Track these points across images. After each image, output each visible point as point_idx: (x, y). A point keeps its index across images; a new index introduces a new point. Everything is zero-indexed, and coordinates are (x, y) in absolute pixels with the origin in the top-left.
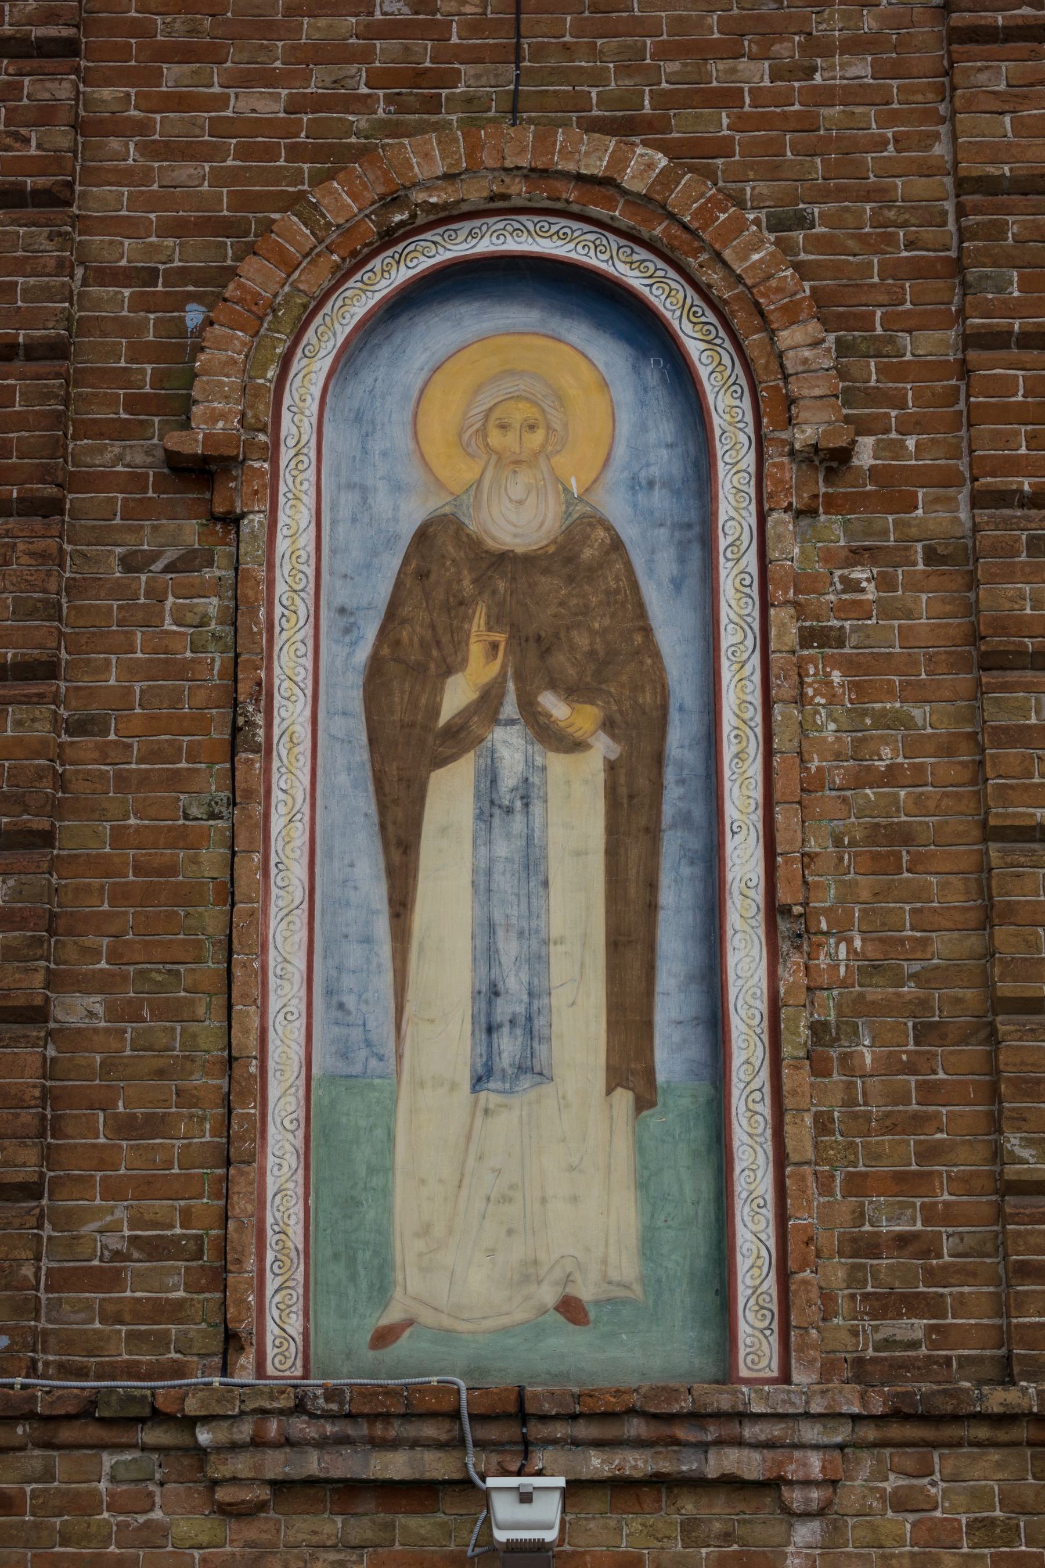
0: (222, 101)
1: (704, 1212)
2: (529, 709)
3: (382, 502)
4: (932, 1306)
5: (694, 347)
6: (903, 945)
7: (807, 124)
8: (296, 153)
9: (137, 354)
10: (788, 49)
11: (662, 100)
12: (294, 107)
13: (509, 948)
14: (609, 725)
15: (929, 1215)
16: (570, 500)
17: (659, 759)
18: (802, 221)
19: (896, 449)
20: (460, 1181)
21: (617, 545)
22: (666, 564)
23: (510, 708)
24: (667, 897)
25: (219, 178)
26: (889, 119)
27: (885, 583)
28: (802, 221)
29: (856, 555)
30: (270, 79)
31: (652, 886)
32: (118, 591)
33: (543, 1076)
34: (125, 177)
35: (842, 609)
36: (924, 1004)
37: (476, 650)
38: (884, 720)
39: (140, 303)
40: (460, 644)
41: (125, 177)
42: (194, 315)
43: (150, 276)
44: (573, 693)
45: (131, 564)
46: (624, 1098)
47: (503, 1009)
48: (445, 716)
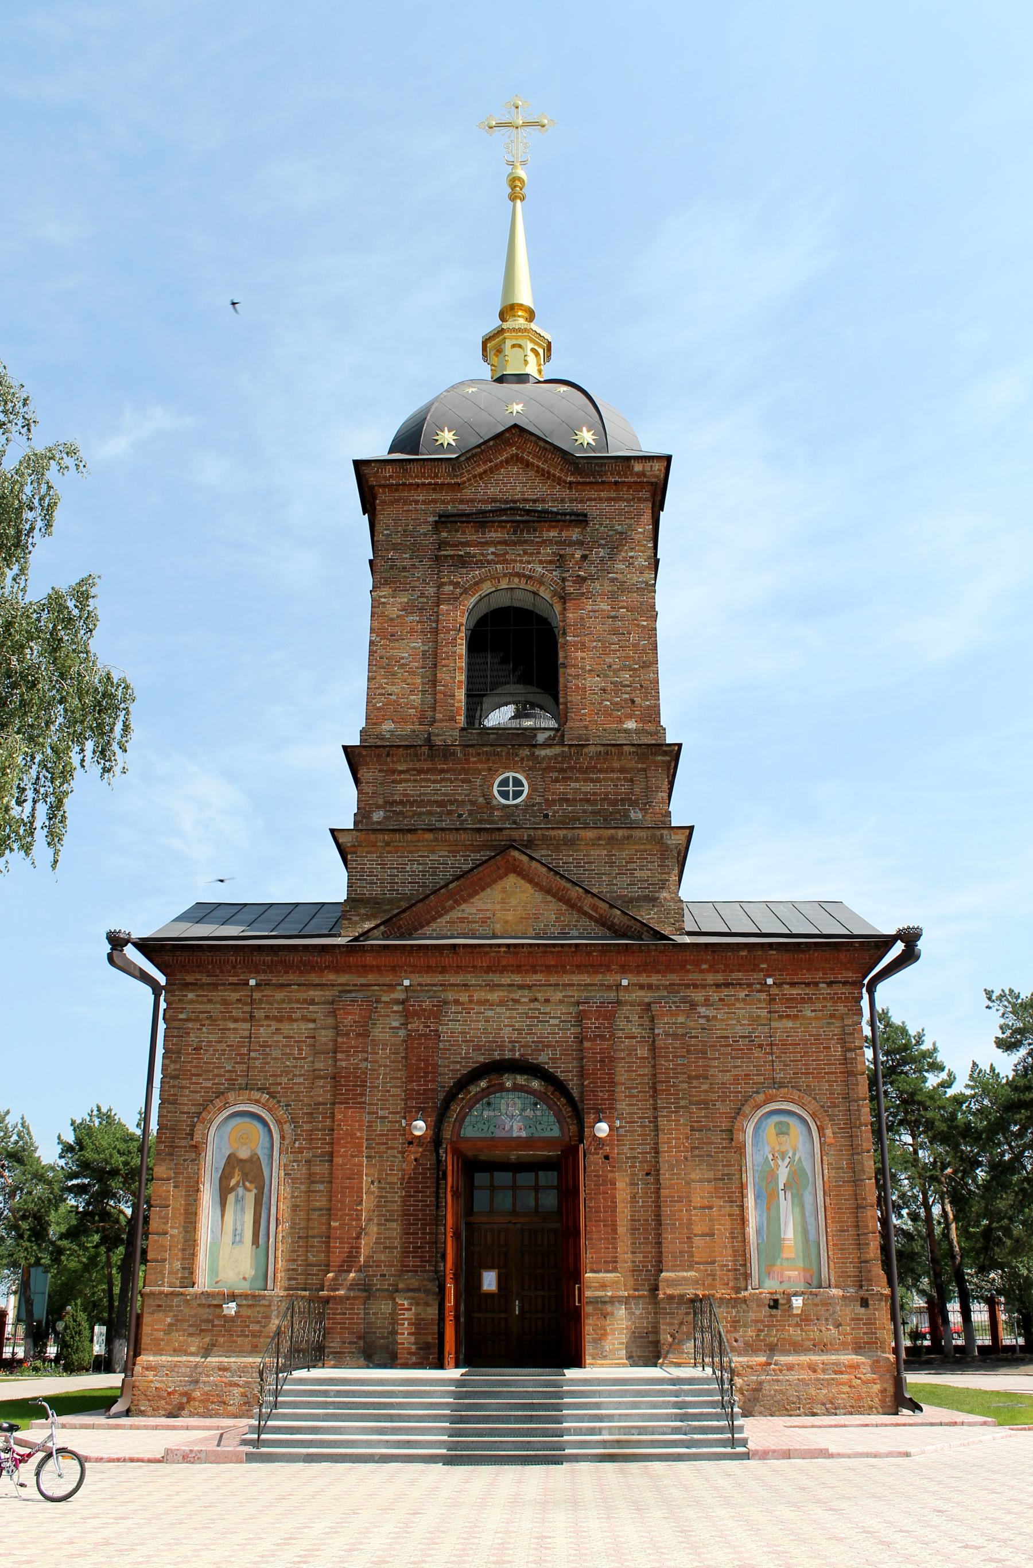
0: (201, 1083)
1: (265, 1264)
2: (244, 1184)
3: (223, 1150)
4: (296, 1279)
5: (272, 1126)
6: (620, 813)
7: (292, 1088)
8: (213, 1092)
9: (187, 1126)
10: (290, 1076)
11: (270, 1084)
12: (213, 1084)
13: (238, 1223)
14: (256, 1188)
15: (297, 1265)
16: (252, 1151)
17: (263, 1193)
18: (290, 1105)
19: (302, 1144)
20: (124, 1460)
21: (259, 1158)
22: (266, 1161)
23: (241, 1184)
24: (263, 1215)
25: (200, 1096)
26: (305, 1088)
27: (298, 1166)
28: (290, 1105)
29: (294, 1161)
30: (209, 1080)
31: (261, 1214)
32: (182, 1165)
33: (243, 1243)
34: (186, 1096)
35: (291, 1170)
36: (299, 1233)
37: (236, 1175)
38: (296, 1188)
39: (187, 1117)
40: (234, 1173)
41: (186, 1096)
42: (196, 1119)
43: (189, 1113)
44: (251, 1182)
45: (185, 1160)
46: (254, 1246)
47: (237, 1232)
48: (231, 1185)
